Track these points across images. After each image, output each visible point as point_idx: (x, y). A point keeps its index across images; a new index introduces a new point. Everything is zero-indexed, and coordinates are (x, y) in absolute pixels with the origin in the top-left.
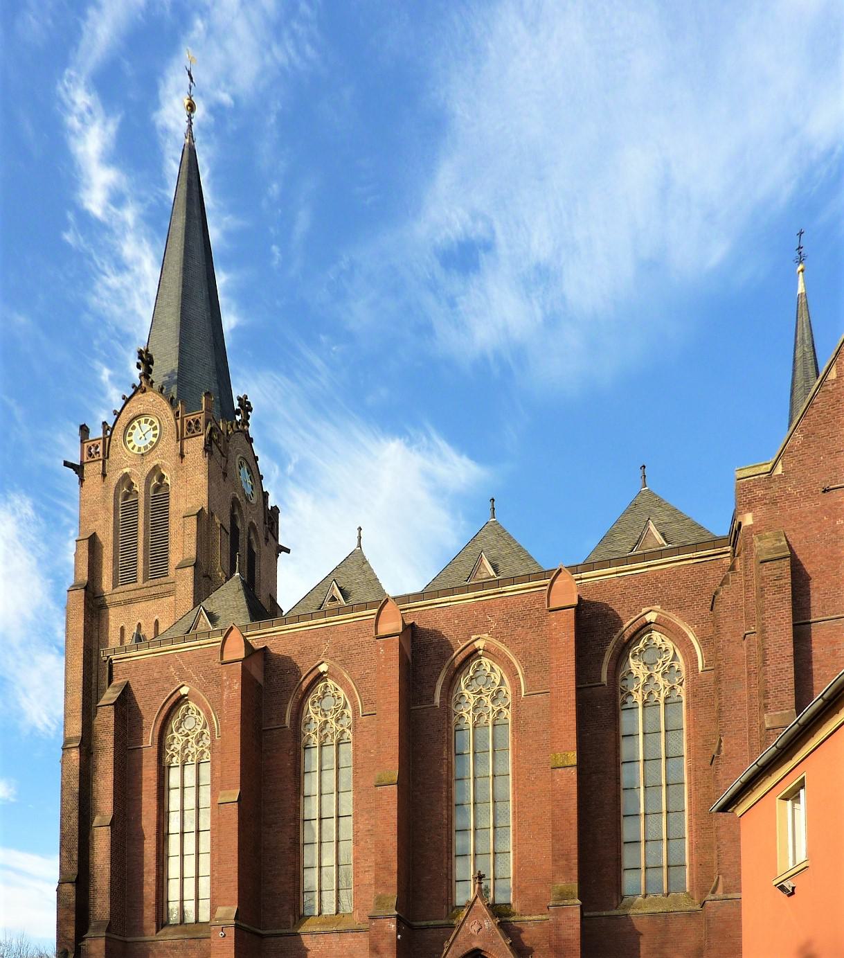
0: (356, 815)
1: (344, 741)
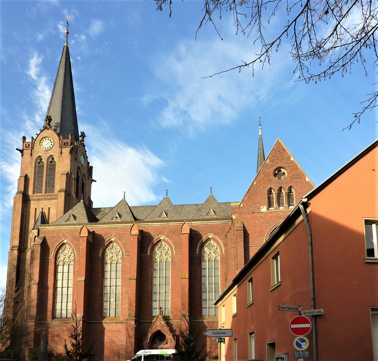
0: (122, 286)
1: (119, 263)
